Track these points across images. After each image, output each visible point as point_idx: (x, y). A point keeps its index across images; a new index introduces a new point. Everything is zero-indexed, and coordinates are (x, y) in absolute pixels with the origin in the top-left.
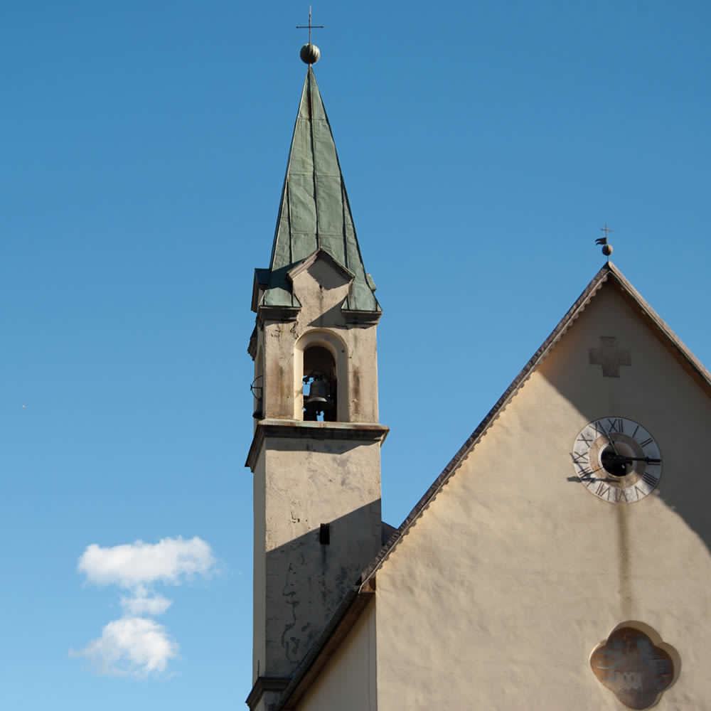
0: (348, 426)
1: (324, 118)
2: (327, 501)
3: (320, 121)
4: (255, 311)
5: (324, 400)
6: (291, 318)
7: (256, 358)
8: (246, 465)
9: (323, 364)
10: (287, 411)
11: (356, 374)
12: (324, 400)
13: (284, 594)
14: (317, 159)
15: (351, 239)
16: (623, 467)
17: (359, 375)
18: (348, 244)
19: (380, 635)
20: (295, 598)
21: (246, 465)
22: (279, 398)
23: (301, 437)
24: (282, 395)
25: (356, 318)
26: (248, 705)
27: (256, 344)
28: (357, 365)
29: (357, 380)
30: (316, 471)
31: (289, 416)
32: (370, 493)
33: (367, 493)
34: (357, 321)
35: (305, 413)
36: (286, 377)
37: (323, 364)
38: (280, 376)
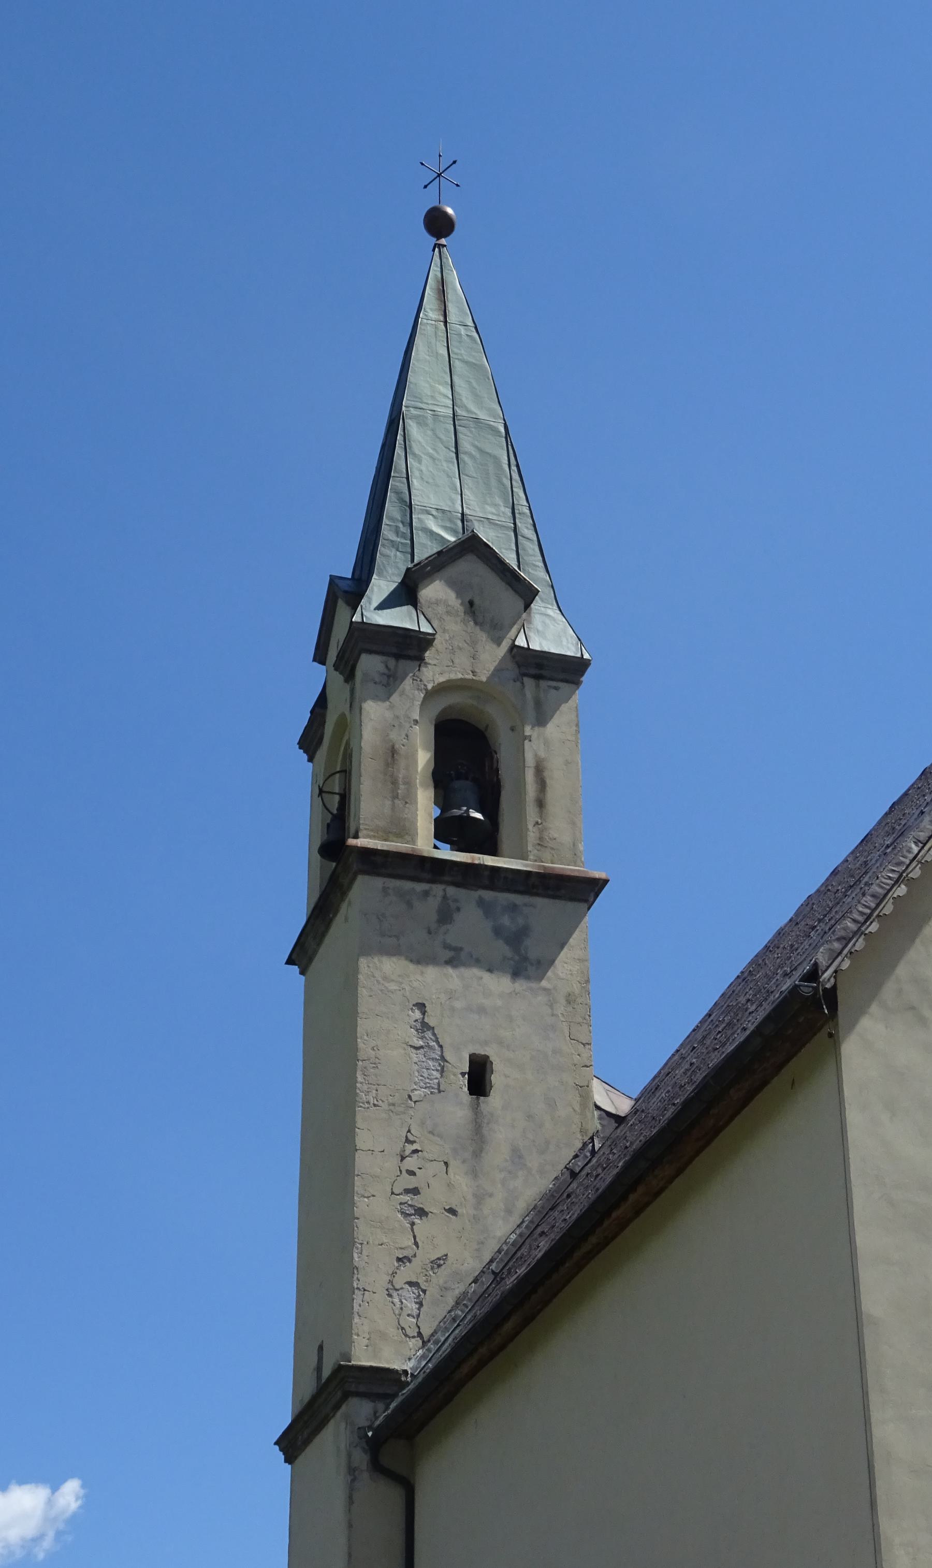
0: (526, 865)
1: (470, 323)
2: (482, 1010)
3: (462, 328)
4: (323, 662)
5: (479, 816)
6: (412, 653)
7: (322, 754)
8: (290, 961)
9: (468, 757)
10: (404, 830)
11: (539, 770)
12: (479, 816)
13: (393, 1193)
14: (457, 388)
15: (526, 530)
16: (370, 1434)
17: (546, 774)
18: (519, 537)
19: (854, 1117)
20: (418, 1201)
21: (290, 961)
22: (388, 803)
23: (432, 881)
24: (395, 797)
25: (539, 666)
26: (281, 1450)
27: (323, 723)
28: (542, 754)
29: (542, 785)
30: (461, 949)
31: (408, 838)
32: (569, 1002)
33: (563, 1001)
34: (544, 672)
35: (582, 675)
36: (402, 763)
37: (468, 757)
38: (390, 760)
